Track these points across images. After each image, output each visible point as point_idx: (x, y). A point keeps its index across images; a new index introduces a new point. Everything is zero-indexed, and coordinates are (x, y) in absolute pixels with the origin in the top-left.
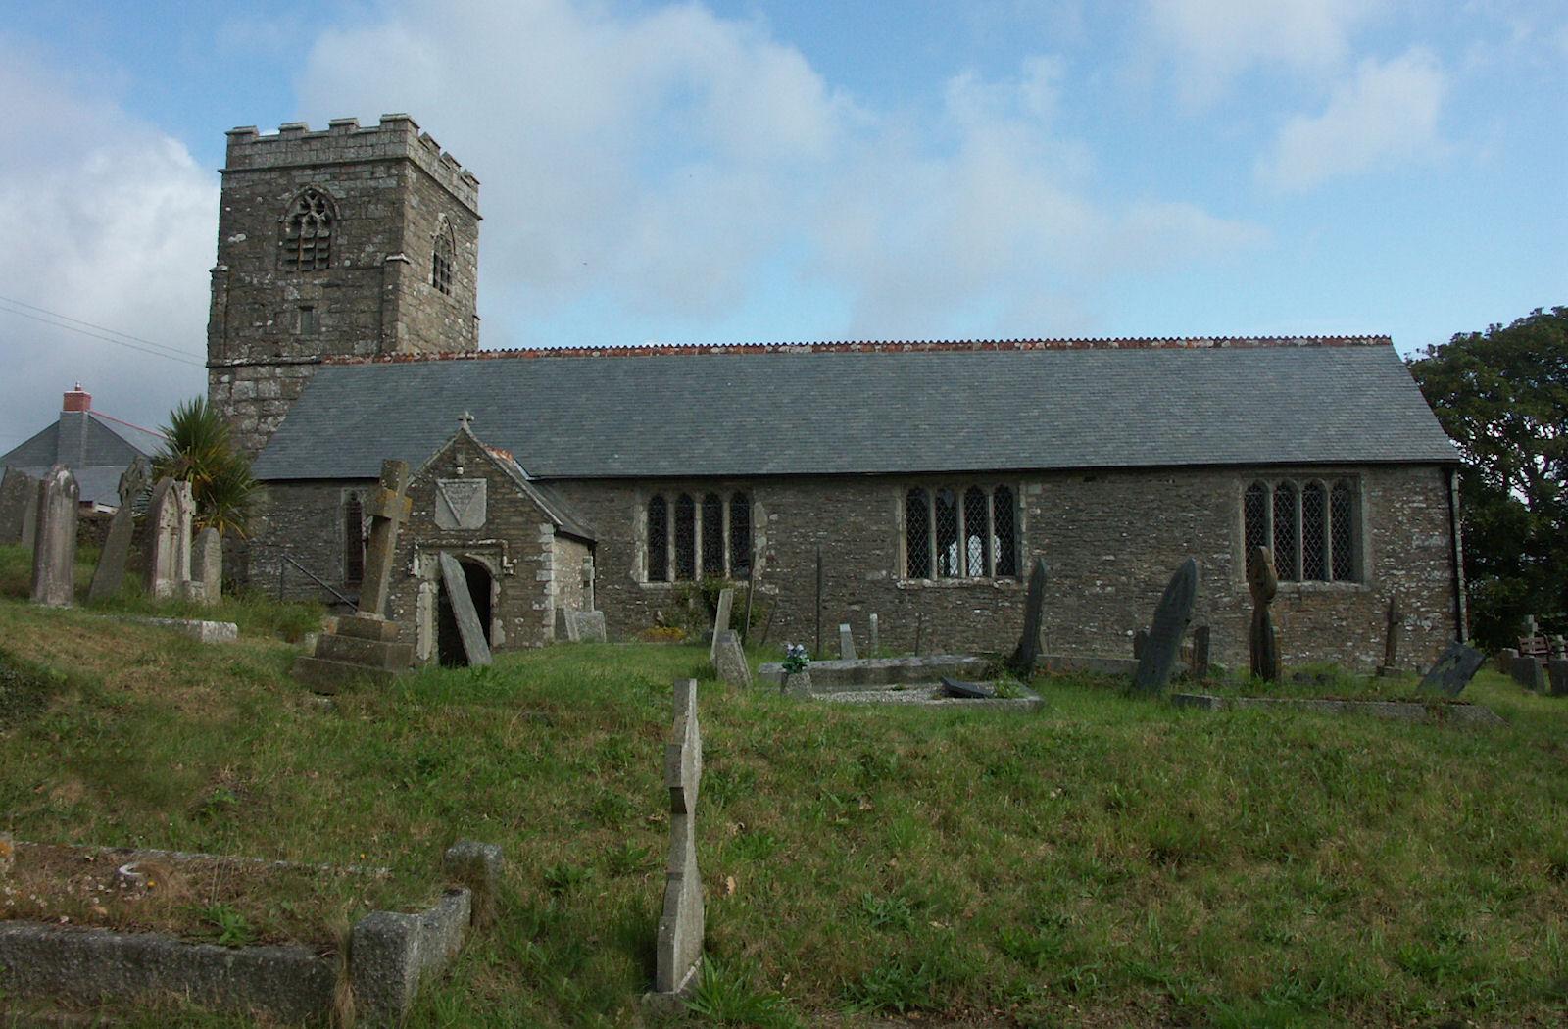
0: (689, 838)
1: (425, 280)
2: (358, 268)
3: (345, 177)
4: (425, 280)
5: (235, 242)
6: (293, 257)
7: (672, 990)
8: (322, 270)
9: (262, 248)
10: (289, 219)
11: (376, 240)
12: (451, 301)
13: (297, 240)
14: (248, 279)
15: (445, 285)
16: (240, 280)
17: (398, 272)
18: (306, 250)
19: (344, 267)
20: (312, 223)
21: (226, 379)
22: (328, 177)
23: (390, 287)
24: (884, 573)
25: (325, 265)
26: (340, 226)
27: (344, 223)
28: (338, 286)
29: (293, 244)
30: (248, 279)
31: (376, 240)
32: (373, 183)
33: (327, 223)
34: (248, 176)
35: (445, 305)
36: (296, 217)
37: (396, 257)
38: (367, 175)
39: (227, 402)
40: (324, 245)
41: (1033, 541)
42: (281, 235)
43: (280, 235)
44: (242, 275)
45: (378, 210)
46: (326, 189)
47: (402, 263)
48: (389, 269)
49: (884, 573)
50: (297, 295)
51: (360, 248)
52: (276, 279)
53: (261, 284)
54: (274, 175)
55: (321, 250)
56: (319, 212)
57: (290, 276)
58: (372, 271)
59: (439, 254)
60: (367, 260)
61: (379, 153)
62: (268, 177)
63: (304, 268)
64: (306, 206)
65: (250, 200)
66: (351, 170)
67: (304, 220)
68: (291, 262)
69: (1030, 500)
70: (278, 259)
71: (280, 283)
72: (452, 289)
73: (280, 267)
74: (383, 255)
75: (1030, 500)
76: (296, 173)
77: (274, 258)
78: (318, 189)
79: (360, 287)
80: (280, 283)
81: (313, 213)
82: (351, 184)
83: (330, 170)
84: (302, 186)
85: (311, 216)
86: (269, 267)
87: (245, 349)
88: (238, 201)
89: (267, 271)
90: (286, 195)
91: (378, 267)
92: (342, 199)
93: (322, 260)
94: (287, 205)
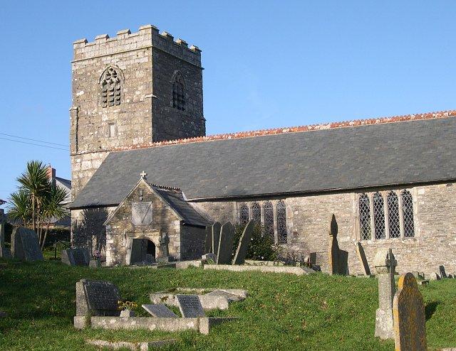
1: (168, 105)
4: (168, 105)
6: (105, 94)
12: (185, 113)
15: (181, 106)
21: (79, 160)
24: (349, 237)
35: (182, 115)
38: (135, 57)
39: (79, 172)
41: (420, 218)
49: (349, 237)
50: (107, 118)
54: (95, 61)
59: (176, 91)
61: (139, 46)
66: (128, 55)
69: (419, 197)
72: (186, 107)
75: (419, 197)
76: (104, 59)
82: (128, 63)
83: (119, 56)
87: (86, 146)
90: (100, 71)
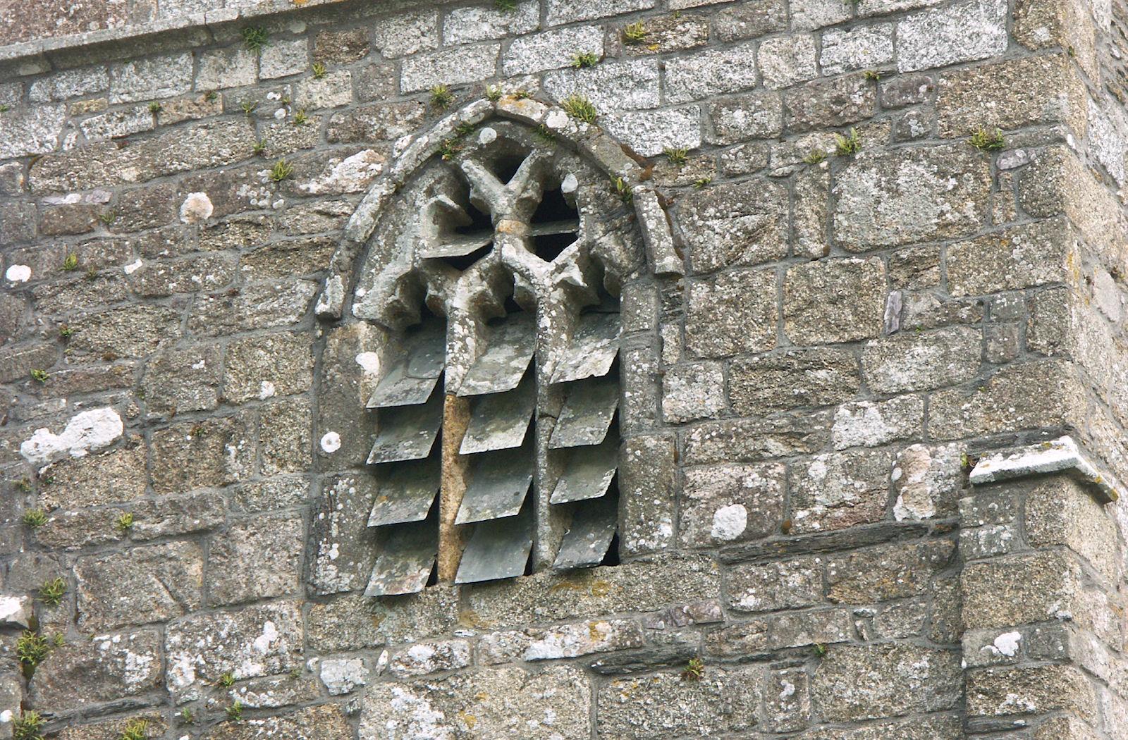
0: (395, 270)
2: (796, 548)
3: (691, 31)
5: (61, 460)
6: (408, 508)
7: (483, 294)
8: (578, 573)
9: (221, 478)
10: (375, 295)
11: (897, 374)
13: (427, 413)
14: (139, 667)
16: (91, 673)
17: (1050, 545)
18: (482, 468)
19: (709, 547)
20: (508, 311)
22: (591, 41)
23: (1008, 643)
25: (592, 548)
26: (674, 308)
27: (699, 293)
28: (681, 661)
29: (401, 449)
30: (139, 667)
31: (897, 374)
32: (863, 48)
33: (595, 305)
34: (131, 82)
36: (413, 283)
37: (1030, 459)
40: (588, 430)
42: (332, 393)
43: (322, 390)
44: (108, 642)
45: (896, 198)
46: (582, 112)
47: (1071, 497)
48: (988, 534)
51: (804, 421)
52: (307, 648)
53: (222, 685)
54: (274, 61)
55: (568, 459)
56: (546, 248)
57: (390, 623)
58: (888, 556)
60: (845, 489)
62: (241, 73)
63: (472, 571)
64: (471, 219)
65: (144, 213)
67: (461, 295)
68: (417, 537)
70: (316, 534)
71: (337, 672)
73: (328, 576)
74: (951, 455)
77: (294, 528)
78: (533, 111)
79: (817, 654)
80: (337, 672)
81: (513, 251)
82: (731, 66)
84: (440, 104)
85: (503, 275)
86: (266, 582)
88: (75, 227)
89: (249, 605)
90: (349, 170)
91: (915, 530)
92: (675, 159)
93: (577, 515)
94: (362, 218)
